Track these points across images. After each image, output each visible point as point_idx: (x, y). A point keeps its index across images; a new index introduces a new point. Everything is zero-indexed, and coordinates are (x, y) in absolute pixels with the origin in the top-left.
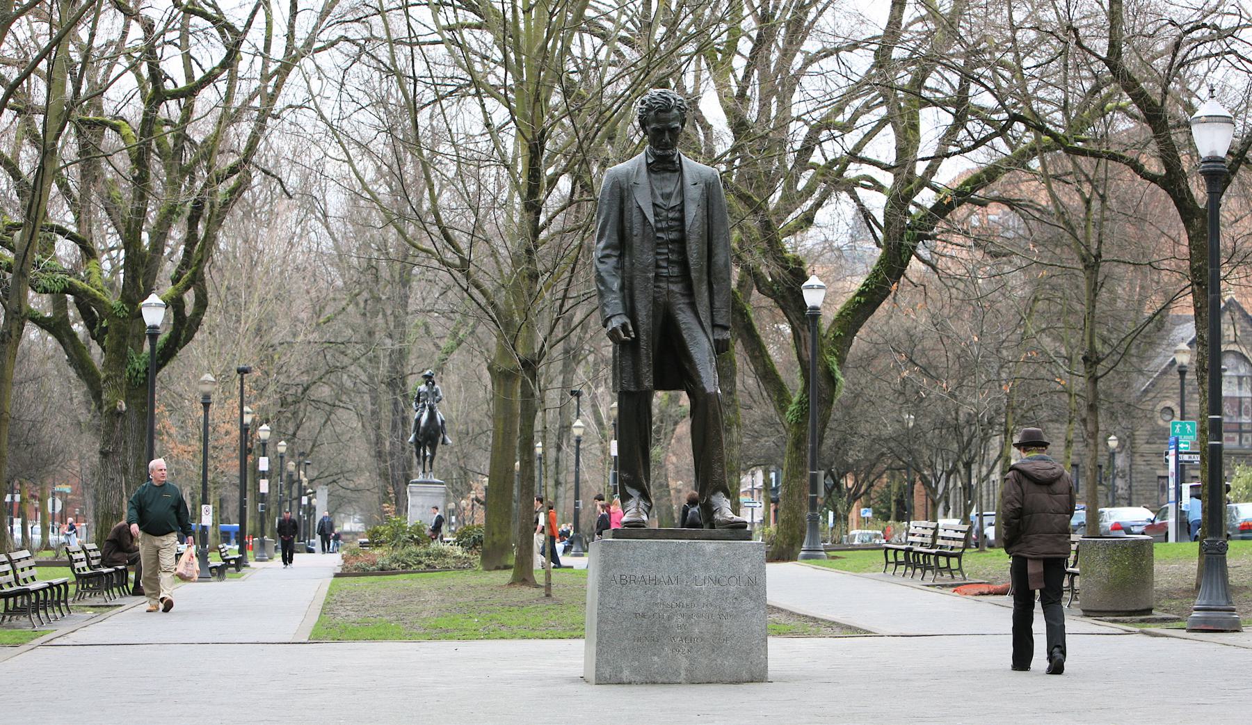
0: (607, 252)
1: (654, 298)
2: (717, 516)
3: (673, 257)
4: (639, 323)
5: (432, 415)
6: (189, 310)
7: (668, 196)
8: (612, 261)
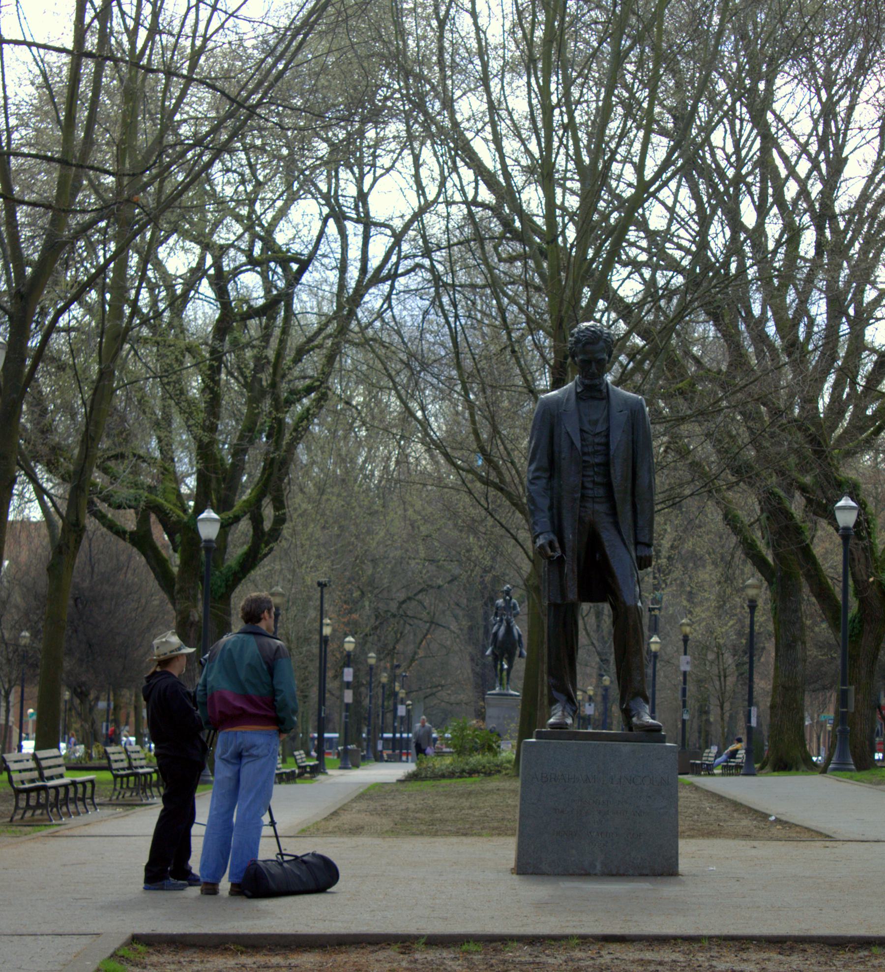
0: (537, 474)
1: (580, 517)
2: (634, 719)
3: (598, 479)
4: (566, 541)
5: (509, 629)
6: (267, 525)
7: (595, 423)
8: (543, 483)
